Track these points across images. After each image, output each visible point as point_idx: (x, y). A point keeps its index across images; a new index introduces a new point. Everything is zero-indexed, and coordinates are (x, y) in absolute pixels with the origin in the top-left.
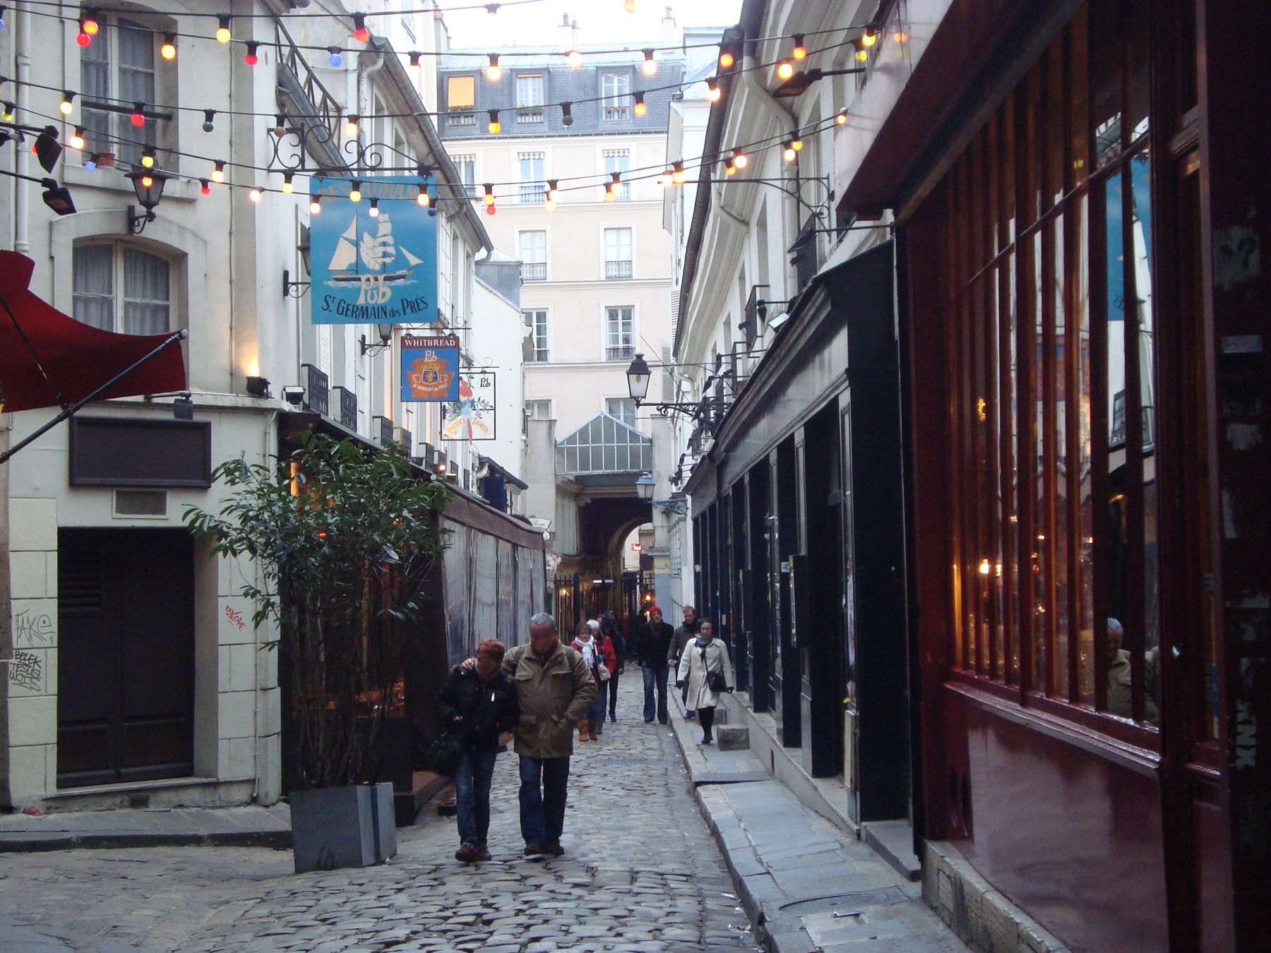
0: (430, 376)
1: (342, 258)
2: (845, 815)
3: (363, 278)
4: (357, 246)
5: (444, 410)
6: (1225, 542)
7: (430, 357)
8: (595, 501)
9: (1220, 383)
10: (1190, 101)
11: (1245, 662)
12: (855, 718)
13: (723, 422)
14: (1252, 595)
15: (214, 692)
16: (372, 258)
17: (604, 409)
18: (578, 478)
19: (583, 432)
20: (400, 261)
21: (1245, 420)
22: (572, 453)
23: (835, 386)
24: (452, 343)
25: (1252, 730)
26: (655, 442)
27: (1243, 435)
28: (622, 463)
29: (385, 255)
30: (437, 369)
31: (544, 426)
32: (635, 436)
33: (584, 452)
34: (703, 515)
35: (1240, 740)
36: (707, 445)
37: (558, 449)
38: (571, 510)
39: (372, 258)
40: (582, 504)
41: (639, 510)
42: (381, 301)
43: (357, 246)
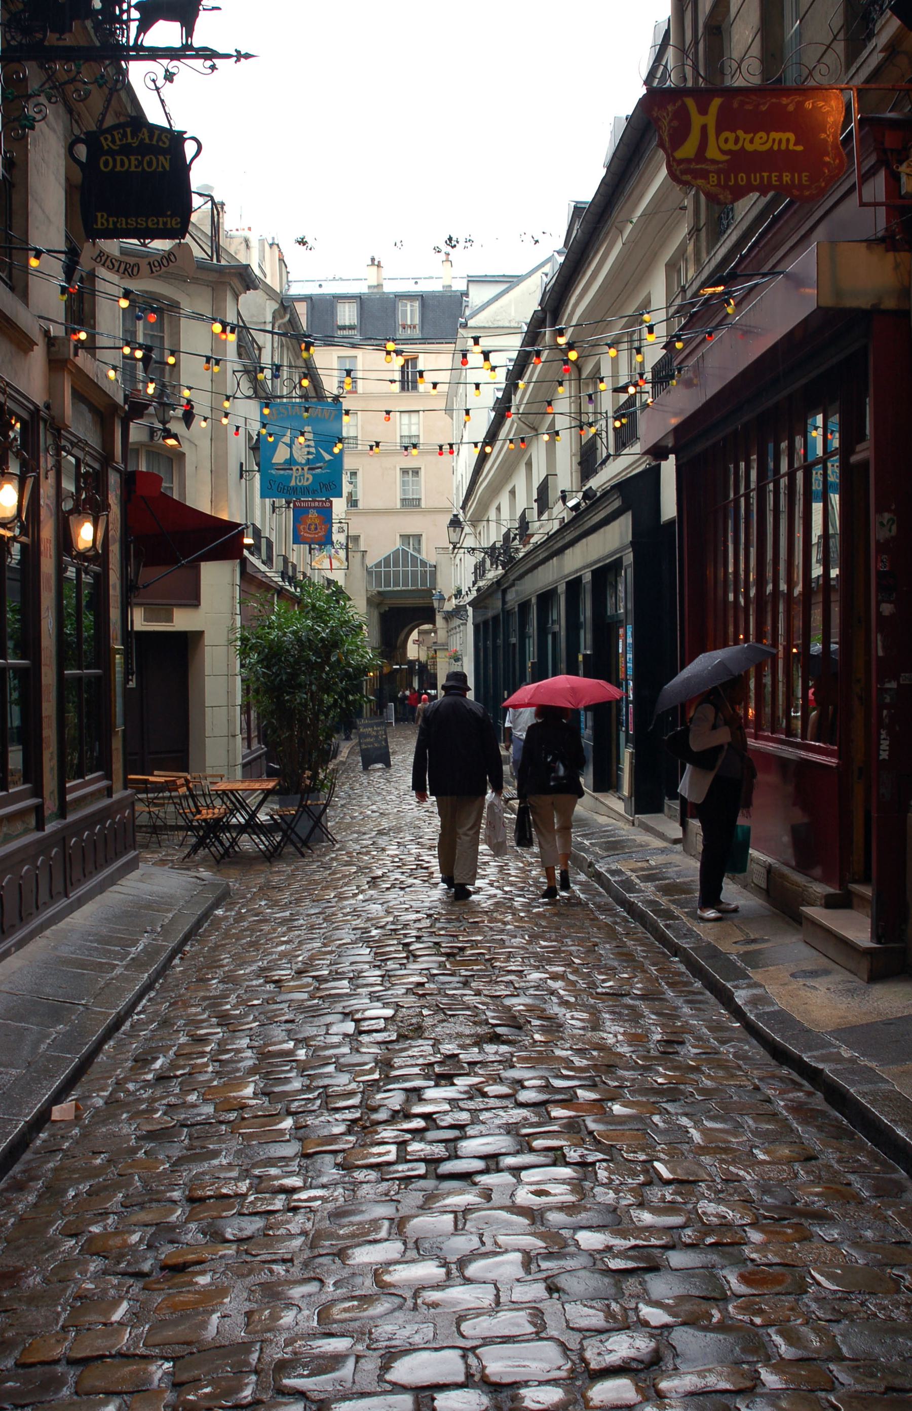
0: (313, 527)
1: (281, 455)
2: (623, 812)
3: (294, 469)
4: (291, 447)
5: (310, 549)
6: (878, 658)
7: (313, 514)
8: (391, 609)
9: (878, 584)
10: (862, 438)
11: (885, 712)
12: (632, 754)
13: (509, 559)
14: (889, 682)
15: (203, 737)
16: (300, 456)
17: (398, 544)
18: (379, 593)
19: (387, 559)
20: (318, 457)
21: (890, 602)
22: (378, 574)
23: (621, 549)
24: (328, 504)
25: (887, 742)
26: (438, 568)
27: (887, 609)
28: (414, 583)
29: (309, 453)
30: (317, 522)
31: (359, 555)
32: (424, 564)
33: (387, 574)
34: (486, 623)
35: (882, 747)
36: (493, 573)
37: (369, 573)
38: (375, 614)
39: (300, 456)
40: (382, 611)
41: (427, 614)
42: (306, 484)
43: (291, 447)
